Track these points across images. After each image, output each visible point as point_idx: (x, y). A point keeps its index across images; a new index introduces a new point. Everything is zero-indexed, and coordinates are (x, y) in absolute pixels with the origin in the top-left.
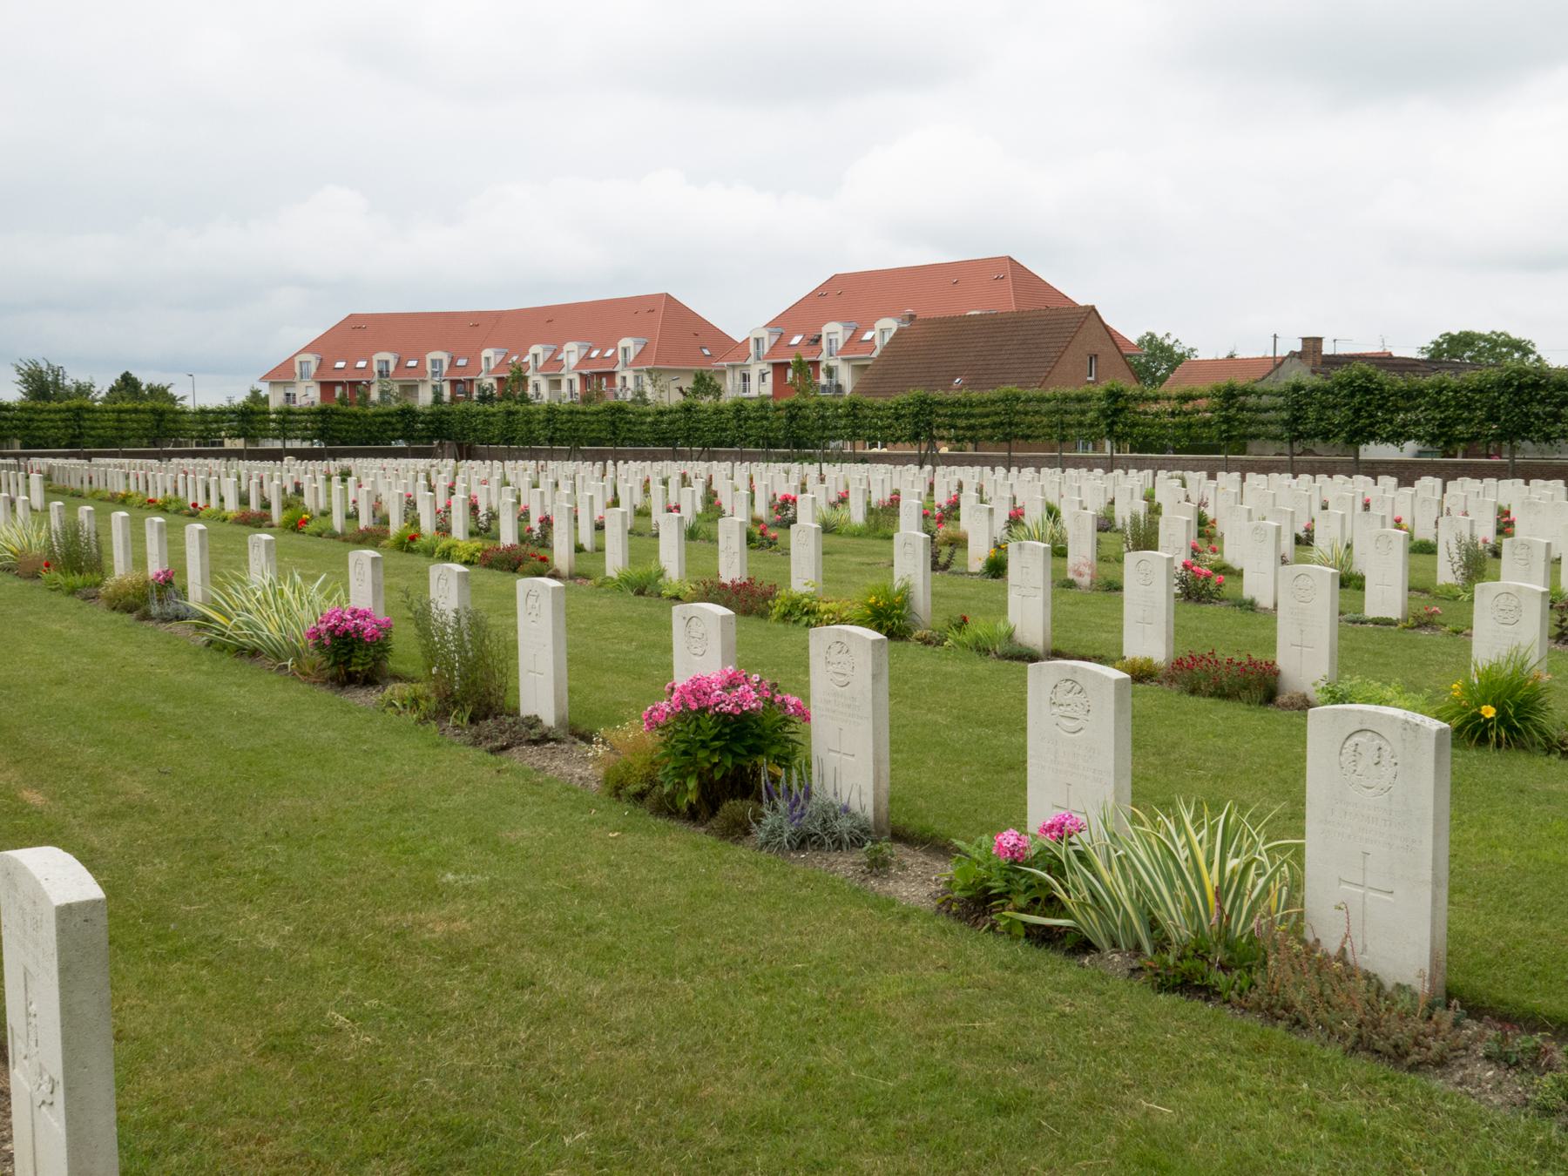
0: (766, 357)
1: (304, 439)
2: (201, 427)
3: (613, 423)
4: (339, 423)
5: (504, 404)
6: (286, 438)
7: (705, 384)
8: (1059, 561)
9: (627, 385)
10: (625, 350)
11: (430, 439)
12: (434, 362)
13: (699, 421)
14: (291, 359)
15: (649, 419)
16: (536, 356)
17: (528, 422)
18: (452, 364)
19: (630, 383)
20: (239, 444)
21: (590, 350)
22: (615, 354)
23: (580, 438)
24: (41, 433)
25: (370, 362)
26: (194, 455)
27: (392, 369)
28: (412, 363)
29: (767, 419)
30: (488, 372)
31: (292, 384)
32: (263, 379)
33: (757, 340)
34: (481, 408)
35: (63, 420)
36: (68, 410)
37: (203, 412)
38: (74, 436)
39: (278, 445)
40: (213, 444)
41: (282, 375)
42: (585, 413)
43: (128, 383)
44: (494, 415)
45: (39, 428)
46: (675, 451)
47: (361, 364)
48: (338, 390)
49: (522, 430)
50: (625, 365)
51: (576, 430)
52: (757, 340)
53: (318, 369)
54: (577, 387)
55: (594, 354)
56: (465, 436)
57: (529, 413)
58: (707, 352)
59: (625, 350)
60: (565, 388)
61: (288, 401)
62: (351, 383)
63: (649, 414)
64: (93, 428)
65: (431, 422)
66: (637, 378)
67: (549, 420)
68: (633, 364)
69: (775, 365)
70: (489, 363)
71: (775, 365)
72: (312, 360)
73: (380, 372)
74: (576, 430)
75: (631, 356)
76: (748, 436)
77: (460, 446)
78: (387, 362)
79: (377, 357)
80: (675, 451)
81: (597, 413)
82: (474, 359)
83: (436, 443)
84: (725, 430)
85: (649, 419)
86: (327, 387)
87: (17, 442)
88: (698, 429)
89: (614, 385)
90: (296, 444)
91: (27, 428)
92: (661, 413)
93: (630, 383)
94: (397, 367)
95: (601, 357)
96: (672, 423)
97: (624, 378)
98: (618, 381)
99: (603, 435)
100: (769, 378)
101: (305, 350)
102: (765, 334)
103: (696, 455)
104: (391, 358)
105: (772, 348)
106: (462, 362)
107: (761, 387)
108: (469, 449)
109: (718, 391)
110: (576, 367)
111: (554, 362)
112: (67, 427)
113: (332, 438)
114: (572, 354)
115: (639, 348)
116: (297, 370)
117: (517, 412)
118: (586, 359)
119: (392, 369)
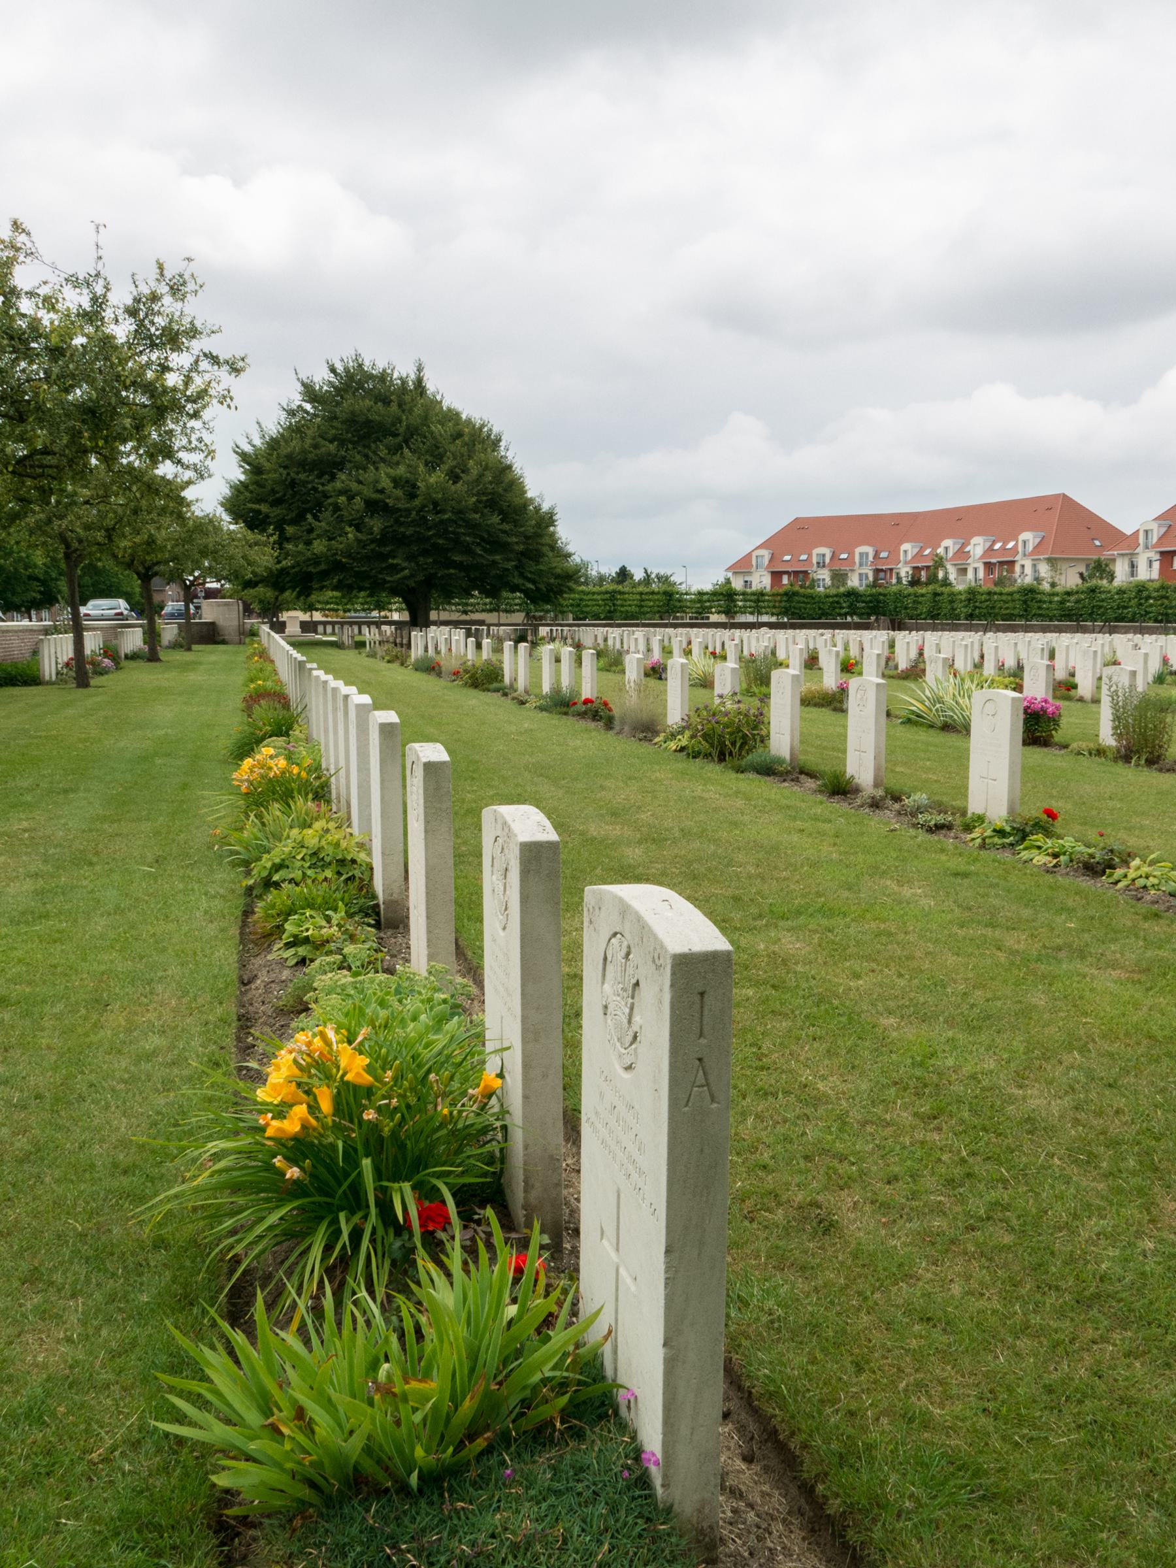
0: (1154, 547)
1: (773, 614)
3: (1025, 602)
4: (799, 602)
5: (931, 587)
6: (760, 613)
7: (1102, 568)
8: (653, 683)
9: (1026, 573)
10: (1025, 542)
11: (869, 615)
12: (861, 554)
13: (1103, 601)
14: (750, 554)
15: (1056, 599)
16: (905, 552)
17: (951, 602)
18: (876, 556)
19: (1028, 570)
20: (722, 618)
21: (994, 543)
22: (1016, 544)
24: (588, 609)
25: (810, 555)
27: (827, 560)
29: (1167, 598)
30: (906, 563)
31: (750, 573)
32: (728, 569)
33: (1146, 532)
34: (911, 590)
36: (607, 593)
37: (700, 593)
38: (610, 612)
39: (751, 619)
40: (702, 618)
41: (743, 566)
42: (1001, 594)
43: (624, 574)
44: (923, 595)
45: (587, 606)
46: (1078, 625)
47: (803, 557)
48: (785, 580)
50: (1025, 555)
51: (993, 608)
52: (1146, 532)
55: (997, 546)
56: (897, 613)
58: (1097, 543)
59: (905, 552)
60: (970, 575)
62: (796, 573)
63: (1057, 595)
64: (622, 606)
65: (871, 602)
66: (1034, 566)
67: (969, 600)
69: (1162, 553)
70: (906, 558)
72: (766, 554)
73: (818, 563)
74: (993, 608)
75: (1030, 547)
76: (1147, 613)
77: (892, 621)
78: (824, 555)
79: (815, 552)
80: (1078, 625)
81: (1011, 594)
83: (873, 618)
84: (1126, 607)
85: (1056, 599)
86: (776, 576)
87: (571, 616)
88: (1101, 607)
89: (1013, 571)
90: (765, 618)
91: (579, 605)
92: (1068, 593)
93: (1028, 570)
94: (831, 559)
95: (1003, 548)
96: (1077, 602)
97: (1023, 566)
98: (1017, 568)
99: (1016, 612)
100: (1156, 565)
102: (1154, 526)
103: (1097, 629)
104: (869, 550)
105: (1160, 539)
106: (884, 555)
107: (1148, 571)
108: (900, 623)
109: (1112, 577)
110: (981, 558)
111: (962, 553)
113: (793, 613)
114: (977, 547)
115: (1038, 540)
119: (827, 560)
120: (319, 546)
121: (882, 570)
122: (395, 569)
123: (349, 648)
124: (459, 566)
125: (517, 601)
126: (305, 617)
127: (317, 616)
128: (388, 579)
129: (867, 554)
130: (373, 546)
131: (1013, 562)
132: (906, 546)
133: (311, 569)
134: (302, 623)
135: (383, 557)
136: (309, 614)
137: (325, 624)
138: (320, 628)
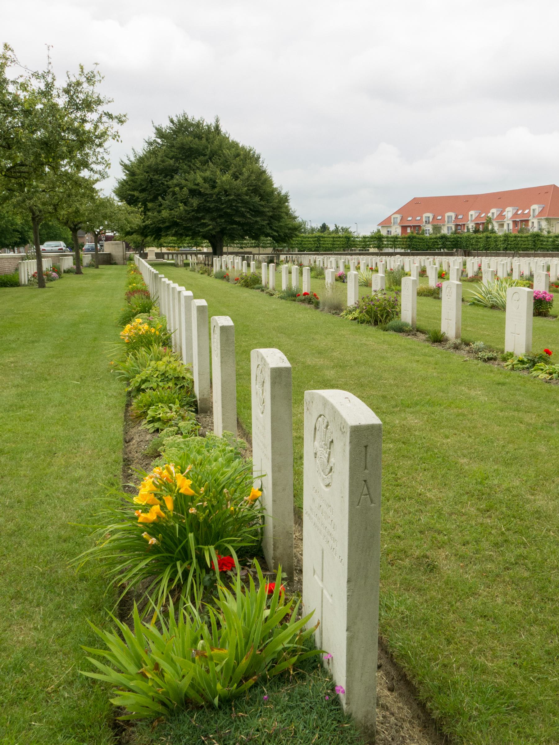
1: (402, 248)
2: (363, 244)
3: (534, 241)
4: (416, 242)
5: (485, 234)
6: (396, 248)
10: (534, 210)
11: (453, 248)
12: (448, 217)
14: (390, 217)
15: (550, 239)
16: (493, 213)
17: (496, 241)
19: (536, 225)
21: (518, 210)
23: (519, 248)
24: (306, 246)
25: (422, 217)
26: (360, 254)
27: (431, 220)
28: (439, 218)
30: (472, 221)
31: (390, 226)
34: (474, 235)
35: (314, 241)
38: (317, 247)
39: (391, 250)
40: (366, 250)
41: (386, 223)
42: (521, 237)
44: (481, 238)
47: (418, 218)
48: (409, 230)
49: (493, 245)
50: (534, 217)
51: (517, 244)
53: (401, 220)
54: (511, 227)
55: (520, 212)
56: (468, 247)
57: (496, 237)
59: (472, 215)
60: (505, 227)
61: (388, 234)
63: (551, 237)
64: (324, 244)
65: (453, 241)
66: (539, 222)
67: (505, 240)
68: (537, 216)
69: (513, 221)
70: (472, 217)
71: (513, 221)
72: (399, 217)
73: (426, 221)
74: (517, 244)
75: (537, 213)
77: (465, 252)
78: (429, 217)
81: (527, 237)
82: (466, 215)
83: (455, 250)
85: (550, 239)
86: (404, 228)
87: (297, 249)
89: (528, 226)
90: (398, 250)
91: (301, 244)
93: (536, 225)
94: (433, 219)
95: (523, 213)
97: (533, 223)
98: (530, 224)
99: (529, 246)
101: (396, 213)
104: (453, 215)
106: (460, 217)
108: (469, 252)
110: (511, 218)
111: (501, 216)
112: (315, 244)
113: (413, 248)
114: (509, 212)
115: (541, 209)
116: (392, 221)
117: (491, 237)
118: (516, 214)
119: (431, 220)
120: (165, 214)
121: (459, 225)
122: (205, 225)
123: (181, 266)
124: (238, 223)
125: (269, 242)
126: (158, 250)
127: (164, 250)
128: (201, 230)
129: (451, 217)
130: (193, 213)
131: (528, 221)
132: (472, 212)
133: (161, 225)
134: (156, 253)
135: (198, 219)
136: (160, 249)
137: (168, 254)
138: (166, 256)
